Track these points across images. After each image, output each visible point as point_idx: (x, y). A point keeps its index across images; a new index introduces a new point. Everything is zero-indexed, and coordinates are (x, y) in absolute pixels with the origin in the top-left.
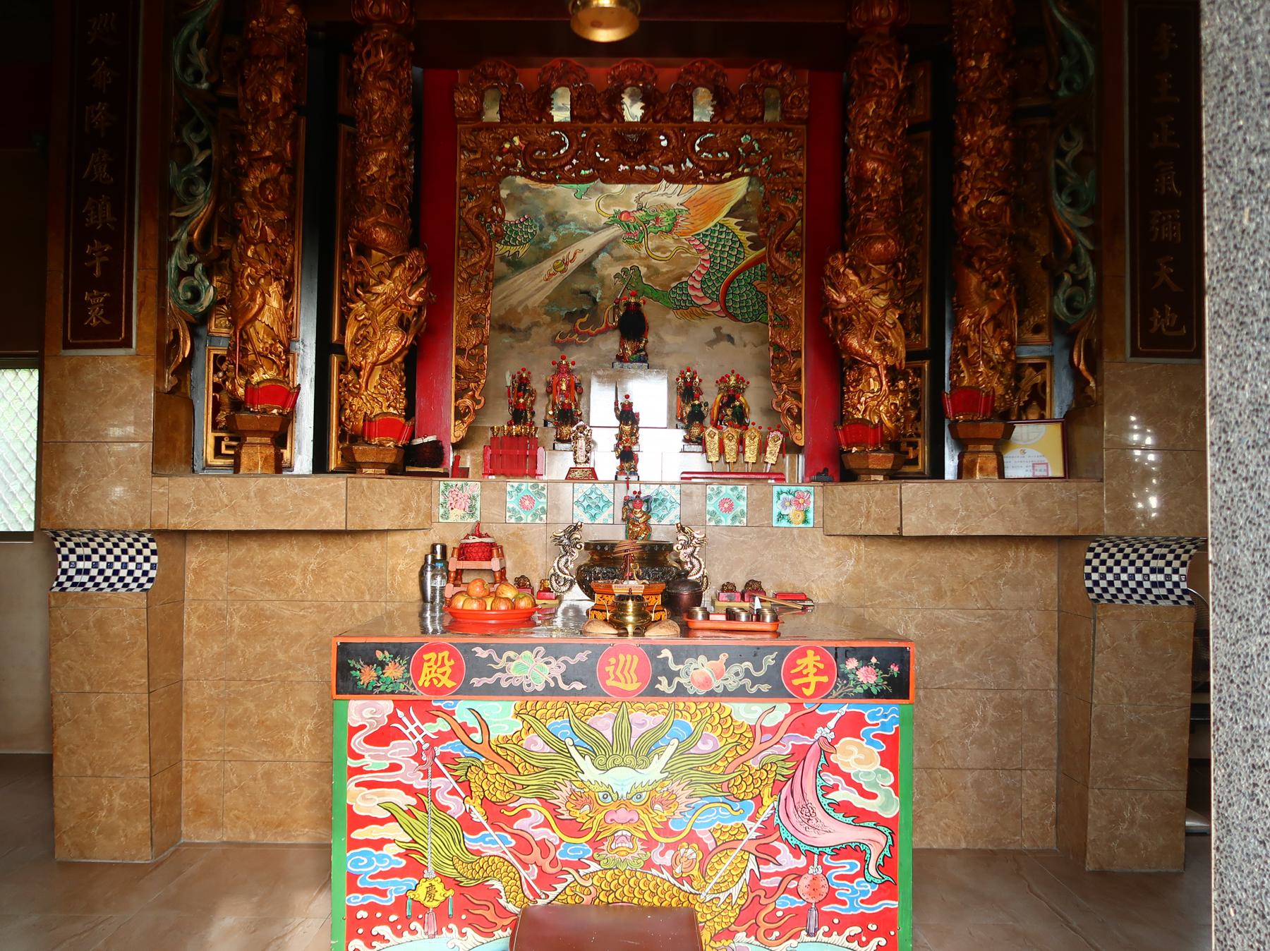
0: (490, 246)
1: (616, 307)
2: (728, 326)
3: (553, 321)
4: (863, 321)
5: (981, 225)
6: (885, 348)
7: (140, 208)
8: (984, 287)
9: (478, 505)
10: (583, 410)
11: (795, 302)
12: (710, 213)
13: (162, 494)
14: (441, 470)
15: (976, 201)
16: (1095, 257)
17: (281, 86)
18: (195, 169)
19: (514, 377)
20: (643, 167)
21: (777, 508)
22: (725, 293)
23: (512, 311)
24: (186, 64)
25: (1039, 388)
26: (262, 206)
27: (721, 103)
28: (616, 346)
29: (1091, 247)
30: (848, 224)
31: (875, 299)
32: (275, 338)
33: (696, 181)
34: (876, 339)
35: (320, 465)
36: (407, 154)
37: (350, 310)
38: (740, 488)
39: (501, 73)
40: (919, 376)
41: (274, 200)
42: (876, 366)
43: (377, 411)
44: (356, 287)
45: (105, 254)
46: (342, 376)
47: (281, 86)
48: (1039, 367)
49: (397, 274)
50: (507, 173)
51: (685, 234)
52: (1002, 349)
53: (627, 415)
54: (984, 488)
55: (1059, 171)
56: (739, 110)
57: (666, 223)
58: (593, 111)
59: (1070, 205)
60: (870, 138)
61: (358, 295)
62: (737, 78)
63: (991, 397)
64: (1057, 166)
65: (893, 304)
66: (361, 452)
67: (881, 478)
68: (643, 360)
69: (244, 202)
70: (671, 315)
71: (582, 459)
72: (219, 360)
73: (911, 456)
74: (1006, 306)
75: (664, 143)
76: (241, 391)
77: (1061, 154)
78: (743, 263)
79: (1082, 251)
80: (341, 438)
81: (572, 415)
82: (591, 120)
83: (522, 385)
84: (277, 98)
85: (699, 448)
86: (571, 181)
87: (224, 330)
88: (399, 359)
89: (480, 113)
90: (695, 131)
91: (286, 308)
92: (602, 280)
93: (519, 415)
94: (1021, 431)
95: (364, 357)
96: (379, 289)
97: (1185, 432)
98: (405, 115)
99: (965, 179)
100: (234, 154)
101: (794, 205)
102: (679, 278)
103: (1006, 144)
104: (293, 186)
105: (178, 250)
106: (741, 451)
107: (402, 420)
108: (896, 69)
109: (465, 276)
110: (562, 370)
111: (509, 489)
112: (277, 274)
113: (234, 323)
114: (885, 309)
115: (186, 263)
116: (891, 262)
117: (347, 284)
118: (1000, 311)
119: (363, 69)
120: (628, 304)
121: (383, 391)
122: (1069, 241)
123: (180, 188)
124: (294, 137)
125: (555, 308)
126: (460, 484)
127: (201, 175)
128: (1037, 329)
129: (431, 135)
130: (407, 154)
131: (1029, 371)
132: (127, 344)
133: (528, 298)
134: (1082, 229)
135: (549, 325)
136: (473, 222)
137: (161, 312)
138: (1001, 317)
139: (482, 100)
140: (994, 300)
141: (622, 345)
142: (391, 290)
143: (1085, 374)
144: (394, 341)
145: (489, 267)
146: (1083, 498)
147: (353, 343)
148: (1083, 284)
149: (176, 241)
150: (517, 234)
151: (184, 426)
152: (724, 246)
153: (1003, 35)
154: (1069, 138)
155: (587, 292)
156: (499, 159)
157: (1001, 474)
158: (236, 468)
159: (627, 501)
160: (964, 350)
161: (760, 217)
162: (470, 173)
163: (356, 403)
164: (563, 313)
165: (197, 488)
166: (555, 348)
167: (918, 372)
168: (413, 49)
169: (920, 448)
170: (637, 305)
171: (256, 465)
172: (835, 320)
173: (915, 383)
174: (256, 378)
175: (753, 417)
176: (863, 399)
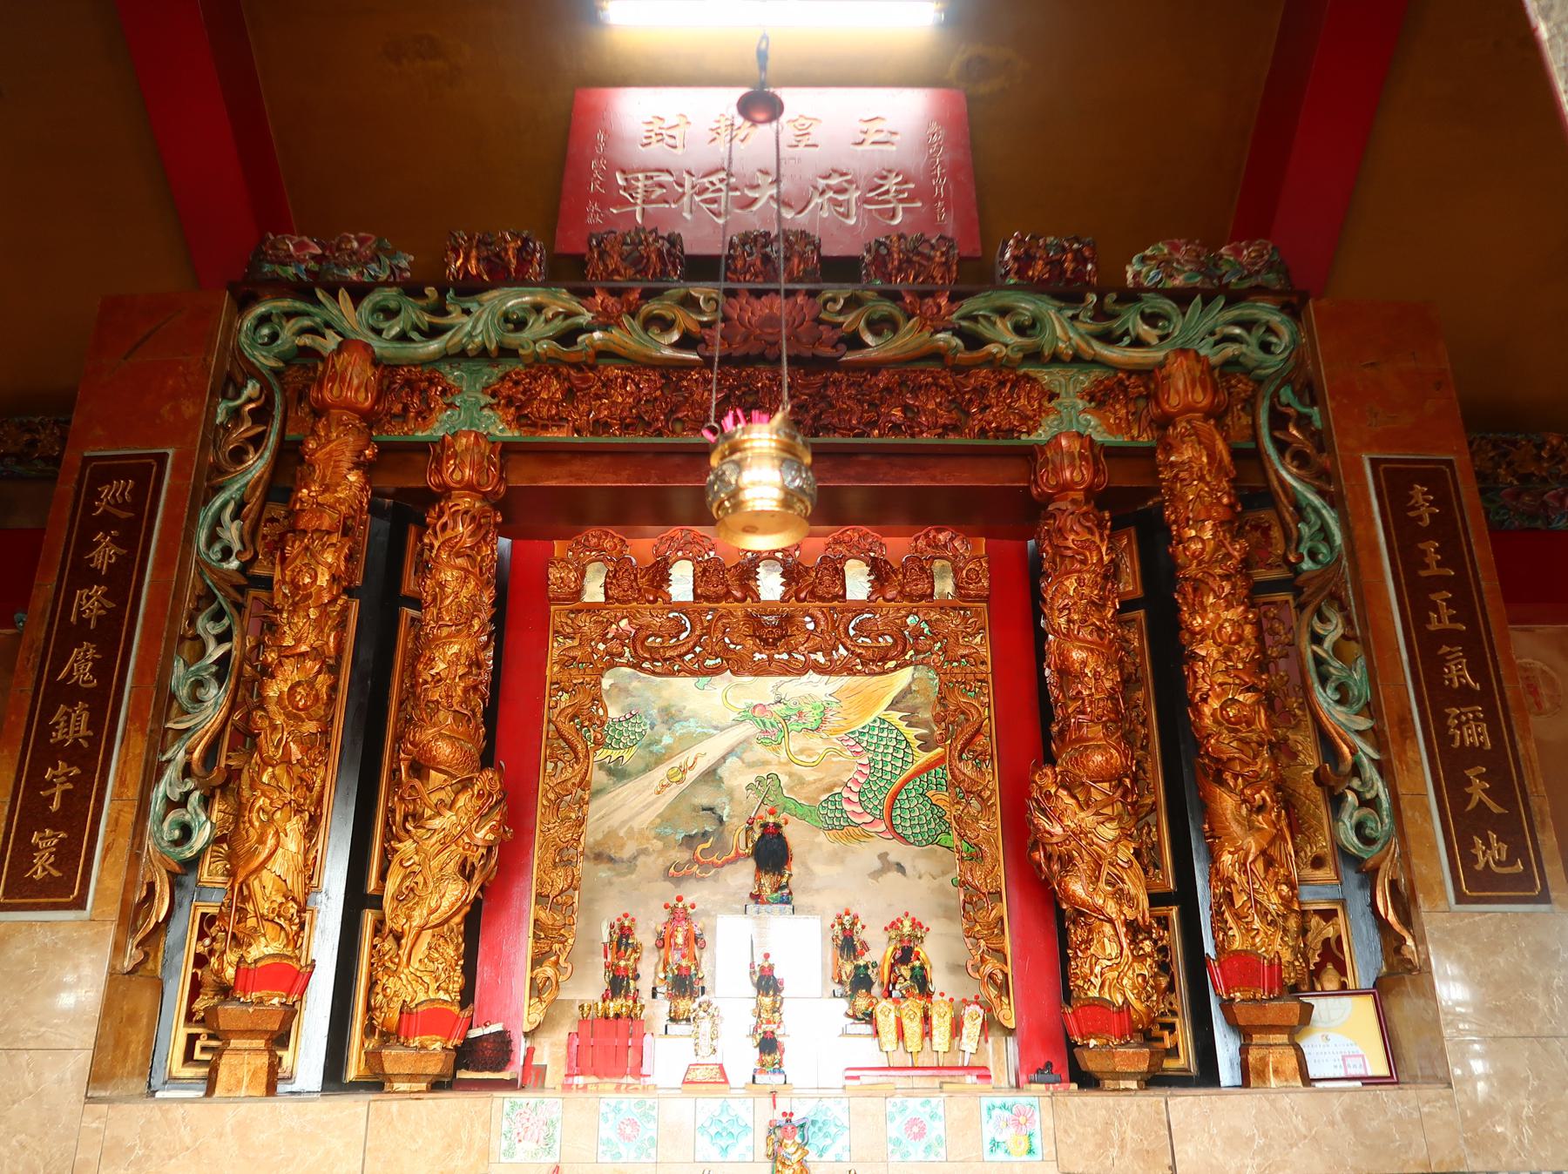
0: (587, 756)
1: (749, 829)
2: (896, 850)
3: (666, 847)
4: (1087, 858)
5: (1231, 731)
6: (1120, 896)
7: (154, 568)
8: (1244, 811)
9: (557, 1136)
10: (705, 970)
11: (990, 827)
12: (867, 705)
13: (97, 1130)
14: (505, 1075)
15: (1219, 695)
16: (1382, 768)
17: (330, 566)
18: (206, 668)
19: (612, 927)
20: (785, 656)
21: (989, 1131)
22: (892, 808)
23: (611, 834)
24: (213, 538)
25: (1333, 942)
26: (288, 716)
27: (880, 573)
28: (750, 880)
29: (1376, 756)
30: (1055, 729)
31: (1100, 829)
32: (288, 896)
33: (852, 672)
34: (1108, 883)
35: (334, 1077)
36: (486, 646)
37: (395, 851)
38: (934, 1101)
39: (607, 544)
40: (1166, 928)
41: (305, 708)
42: (1111, 921)
43: (421, 997)
44: (405, 819)
45: (70, 779)
46: (377, 940)
47: (330, 566)
48: (1328, 915)
49: (460, 803)
50: (611, 665)
51: (836, 732)
52: (1281, 897)
53: (767, 983)
54: (1285, 1101)
55: (1319, 661)
56: (903, 586)
57: (812, 720)
58: (721, 589)
59: (1339, 702)
60: (1074, 622)
61: (408, 831)
62: (898, 547)
63: (1276, 966)
64: (1315, 654)
65: (1125, 835)
66: (395, 1059)
67: (1133, 1085)
68: (786, 901)
69: (265, 710)
70: (822, 837)
71: (705, 1050)
72: (208, 921)
73: (1168, 1043)
74: (1278, 838)
75: (811, 626)
76: (230, 972)
77: (1317, 639)
78: (911, 769)
79: (1365, 760)
80: (369, 1030)
81: (692, 983)
82: (718, 599)
83: (623, 937)
84: (323, 580)
85: (868, 1029)
86: (693, 673)
87: (220, 879)
88: (457, 919)
89: (579, 593)
90: (849, 611)
91: (307, 851)
92: (731, 794)
93: (618, 984)
94: (1323, 1007)
95: (409, 918)
96: (436, 823)
97: (1551, 1010)
98: (485, 599)
99: (1201, 672)
100: (259, 645)
101: (982, 705)
102: (830, 789)
103: (1248, 629)
104: (333, 688)
105: (171, 773)
106: (927, 1034)
107: (456, 1009)
108: (1097, 539)
109: (552, 796)
110: (678, 915)
111: (604, 1109)
112: (299, 805)
113: (231, 874)
114: (1115, 842)
115: (178, 791)
116: (1116, 779)
117: (393, 811)
118: (1272, 843)
119: (436, 545)
120: (765, 826)
121: (432, 967)
122: (1346, 750)
123: (183, 692)
124: (341, 625)
125: (669, 830)
126: (532, 1102)
127: (213, 675)
128: (1318, 863)
129: (517, 610)
130: (486, 646)
131: (1315, 921)
132: (80, 904)
133: (632, 818)
134: (1359, 733)
135: (661, 853)
136: (567, 728)
137: (135, 858)
138: (1271, 851)
139: (583, 575)
140: (1260, 829)
141: (758, 880)
142: (449, 825)
143: (1398, 927)
144: (452, 894)
145: (584, 784)
146: (1429, 1114)
147: (395, 898)
148: (1373, 804)
149: (169, 761)
150: (621, 734)
151: (145, 1021)
152: (886, 746)
153: (1225, 500)
154: (1323, 619)
155: (711, 809)
156: (601, 646)
157: (1307, 1080)
158: (210, 1083)
159: (774, 1127)
160: (1229, 898)
161: (949, 725)
162: (564, 665)
163: (391, 983)
164: (680, 837)
165: (149, 1121)
166: (668, 885)
167: (1164, 922)
168: (499, 519)
169: (1178, 1031)
170: (777, 826)
171: (239, 1082)
172: (1049, 857)
173: (1162, 938)
174: (254, 953)
175: (939, 981)
176: (1097, 970)
